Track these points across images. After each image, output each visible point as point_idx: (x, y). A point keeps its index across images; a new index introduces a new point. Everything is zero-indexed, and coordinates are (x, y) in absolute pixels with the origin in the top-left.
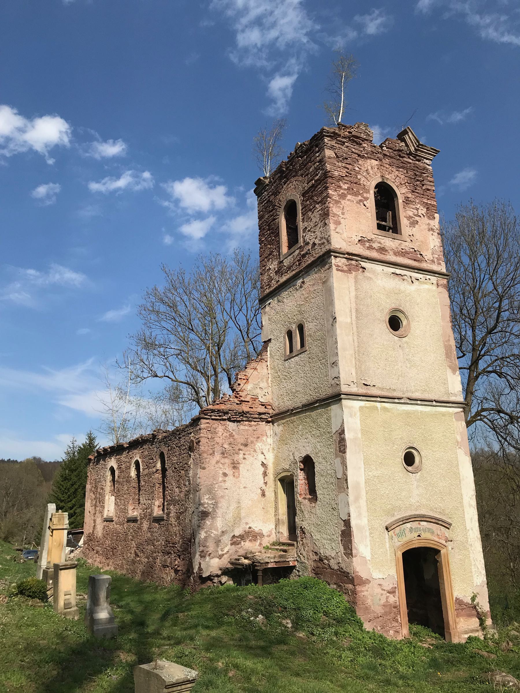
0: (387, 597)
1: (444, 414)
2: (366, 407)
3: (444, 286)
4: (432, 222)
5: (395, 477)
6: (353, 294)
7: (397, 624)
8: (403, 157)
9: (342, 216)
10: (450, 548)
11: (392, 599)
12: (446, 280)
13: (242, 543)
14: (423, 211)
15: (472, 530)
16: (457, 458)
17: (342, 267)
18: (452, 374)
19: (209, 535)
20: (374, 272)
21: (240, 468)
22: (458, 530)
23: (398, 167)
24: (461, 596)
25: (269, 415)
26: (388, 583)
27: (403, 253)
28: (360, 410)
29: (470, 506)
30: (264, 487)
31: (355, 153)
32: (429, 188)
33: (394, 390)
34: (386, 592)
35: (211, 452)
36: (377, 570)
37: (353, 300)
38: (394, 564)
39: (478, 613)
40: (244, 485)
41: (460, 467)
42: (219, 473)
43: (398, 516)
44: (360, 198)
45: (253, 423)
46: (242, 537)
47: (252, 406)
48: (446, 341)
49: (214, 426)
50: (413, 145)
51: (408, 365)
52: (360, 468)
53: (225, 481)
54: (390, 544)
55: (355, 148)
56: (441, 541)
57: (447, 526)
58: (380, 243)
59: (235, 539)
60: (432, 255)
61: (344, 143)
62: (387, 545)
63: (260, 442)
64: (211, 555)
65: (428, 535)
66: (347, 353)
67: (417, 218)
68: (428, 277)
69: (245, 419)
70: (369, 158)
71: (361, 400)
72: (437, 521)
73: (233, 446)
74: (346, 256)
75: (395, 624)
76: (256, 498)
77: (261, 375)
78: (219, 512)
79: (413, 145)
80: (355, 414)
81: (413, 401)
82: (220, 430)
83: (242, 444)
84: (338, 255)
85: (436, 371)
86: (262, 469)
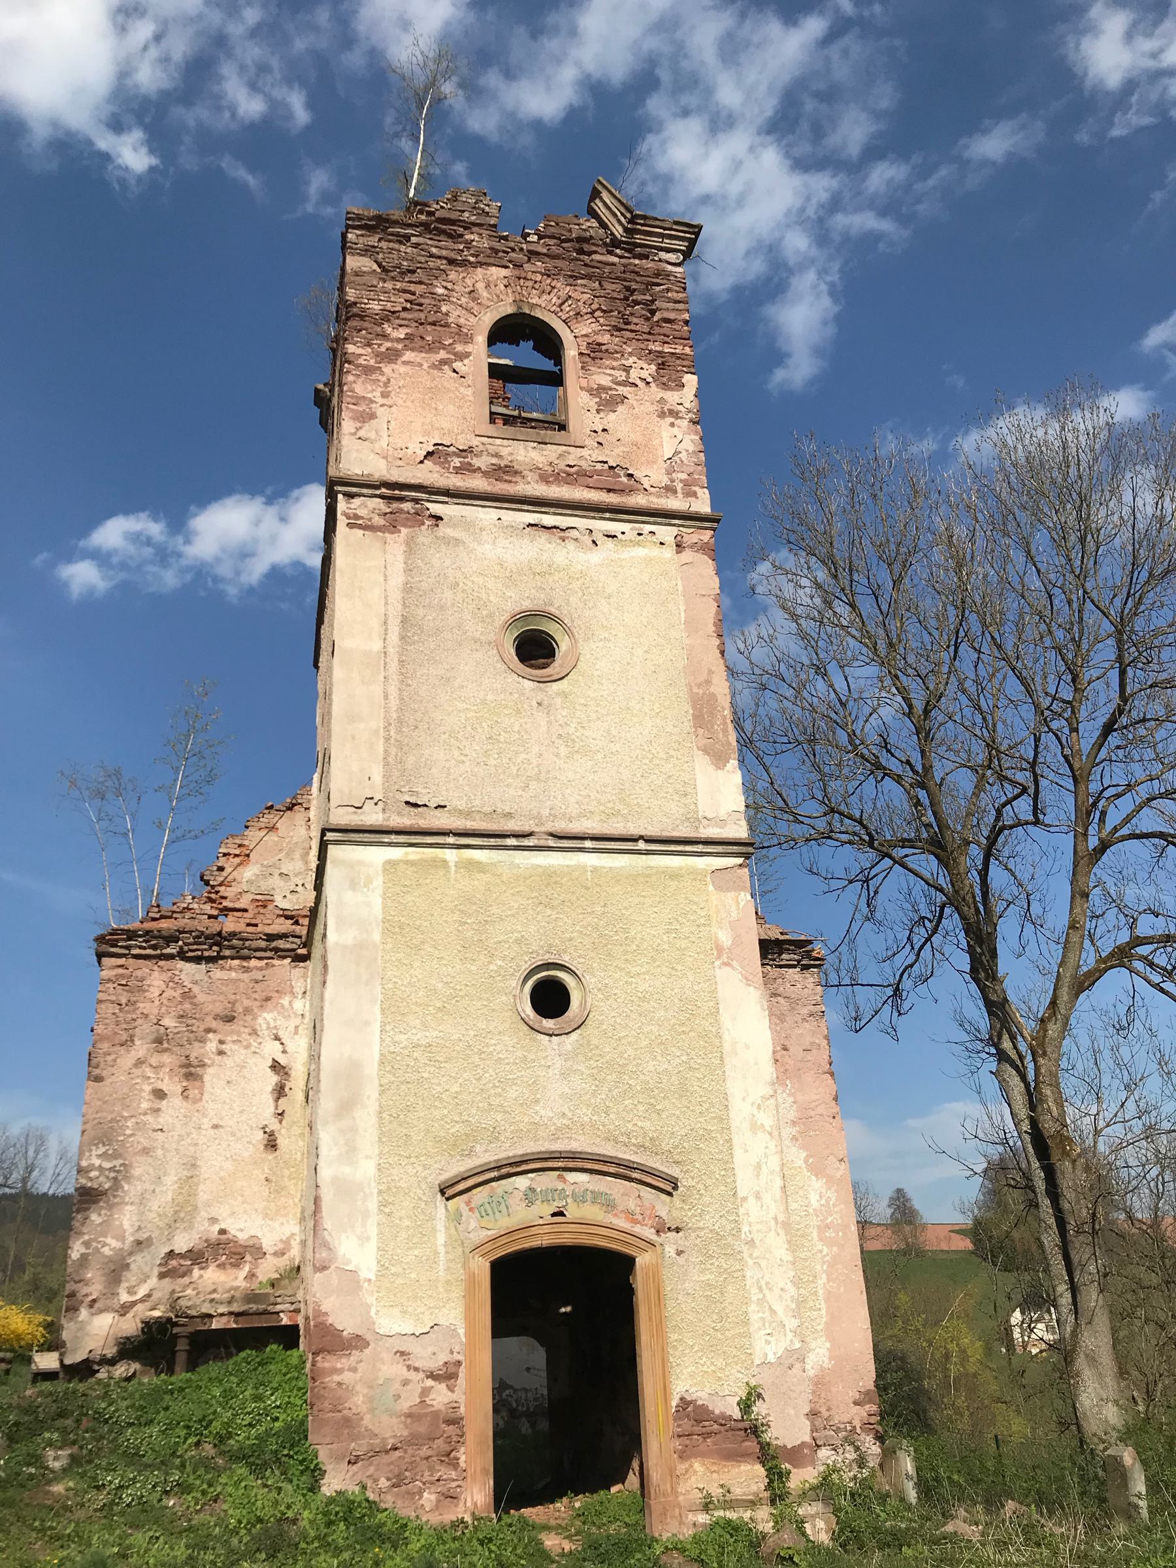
0: (426, 1392)
1: (675, 875)
2: (407, 862)
3: (703, 548)
4: (672, 397)
5: (488, 1045)
7: (454, 1475)
8: (590, 254)
9: (381, 401)
10: (670, 1250)
11: (440, 1396)
12: (710, 533)
13: (196, 1272)
14: (644, 370)
15: (758, 1197)
16: (715, 991)
17: (370, 519)
19: (97, 1250)
20: (467, 524)
21: (206, 1078)
22: (707, 1199)
23: (571, 276)
24: (701, 1394)
25: (297, 941)
26: (431, 1349)
27: (573, 476)
28: (385, 870)
30: (274, 1125)
31: (440, 257)
32: (672, 316)
34: (421, 1375)
36: (396, 1311)
37: (396, 596)
38: (458, 1292)
39: (764, 1447)
41: (725, 1017)
42: (142, 1090)
43: (486, 1155)
44: (443, 354)
45: (253, 963)
46: (196, 1257)
47: (253, 922)
48: (699, 686)
49: (139, 973)
50: (619, 221)
52: (367, 1023)
53: (158, 1110)
54: (449, 1236)
55: (444, 247)
56: (637, 1229)
57: (669, 1186)
58: (497, 455)
59: (174, 1263)
60: (668, 473)
61: (408, 238)
62: (441, 1239)
63: (271, 1011)
64: (97, 1305)
67: (622, 390)
68: (648, 528)
69: (227, 953)
70: (481, 264)
71: (390, 844)
72: (624, 1171)
73: (190, 1022)
74: (384, 490)
75: (444, 1472)
76: (246, 1154)
77: (289, 843)
78: (131, 1190)
79: (619, 221)
80: (369, 881)
81: (605, 841)
82: (156, 983)
84: (354, 490)
85: (656, 761)
86: (274, 1079)
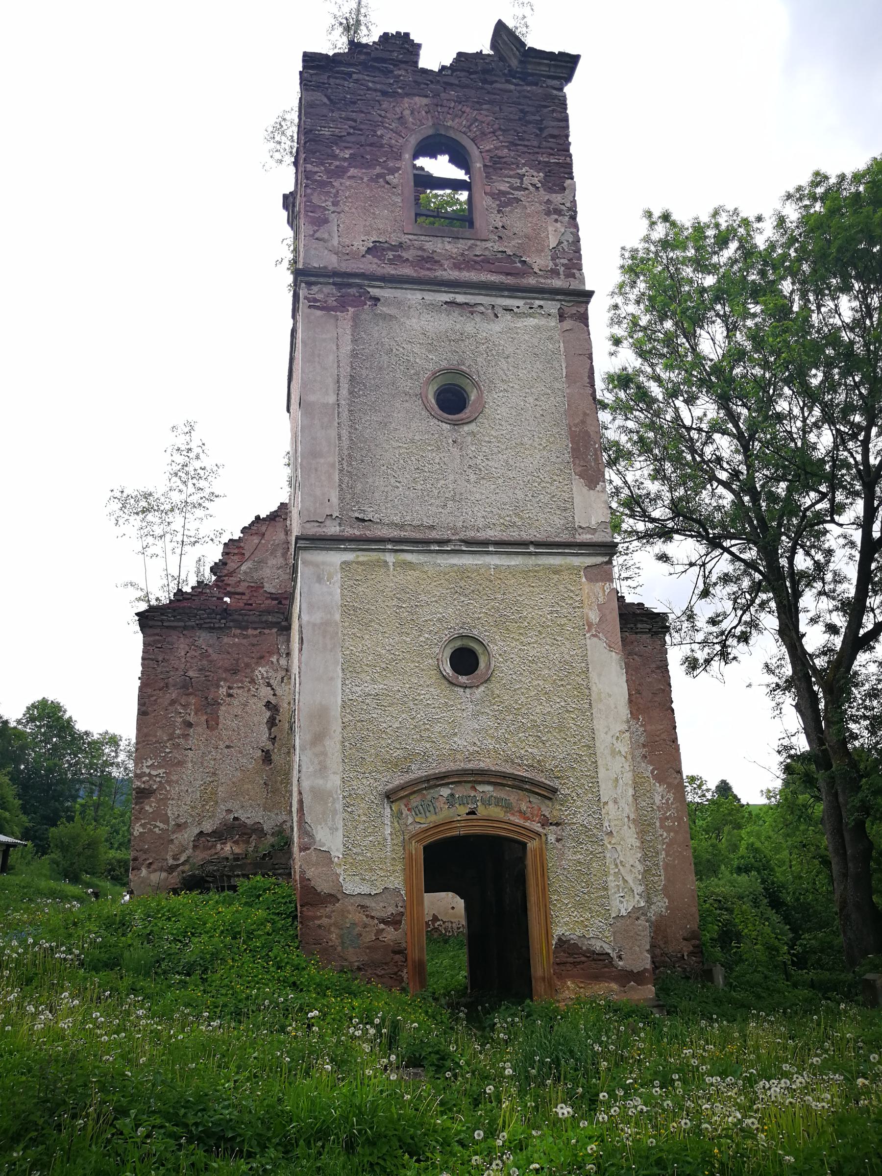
2: (358, 563)
5: (419, 694)
6: (347, 347)
9: (332, 208)
10: (552, 838)
13: (219, 846)
18: (585, 489)
20: (399, 303)
22: (579, 803)
29: (614, 753)
33: (432, 527)
35: (162, 685)
37: (345, 361)
40: (227, 743)
41: (593, 675)
44: (378, 170)
49: (169, 639)
51: (473, 477)
52: (332, 679)
57: (549, 793)
65: (496, 812)
66: (322, 461)
68: (538, 302)
72: (519, 783)
83: (226, 670)
84: (313, 279)
